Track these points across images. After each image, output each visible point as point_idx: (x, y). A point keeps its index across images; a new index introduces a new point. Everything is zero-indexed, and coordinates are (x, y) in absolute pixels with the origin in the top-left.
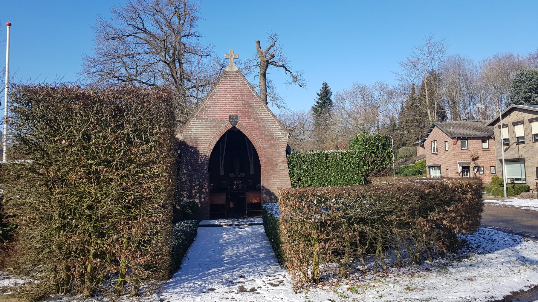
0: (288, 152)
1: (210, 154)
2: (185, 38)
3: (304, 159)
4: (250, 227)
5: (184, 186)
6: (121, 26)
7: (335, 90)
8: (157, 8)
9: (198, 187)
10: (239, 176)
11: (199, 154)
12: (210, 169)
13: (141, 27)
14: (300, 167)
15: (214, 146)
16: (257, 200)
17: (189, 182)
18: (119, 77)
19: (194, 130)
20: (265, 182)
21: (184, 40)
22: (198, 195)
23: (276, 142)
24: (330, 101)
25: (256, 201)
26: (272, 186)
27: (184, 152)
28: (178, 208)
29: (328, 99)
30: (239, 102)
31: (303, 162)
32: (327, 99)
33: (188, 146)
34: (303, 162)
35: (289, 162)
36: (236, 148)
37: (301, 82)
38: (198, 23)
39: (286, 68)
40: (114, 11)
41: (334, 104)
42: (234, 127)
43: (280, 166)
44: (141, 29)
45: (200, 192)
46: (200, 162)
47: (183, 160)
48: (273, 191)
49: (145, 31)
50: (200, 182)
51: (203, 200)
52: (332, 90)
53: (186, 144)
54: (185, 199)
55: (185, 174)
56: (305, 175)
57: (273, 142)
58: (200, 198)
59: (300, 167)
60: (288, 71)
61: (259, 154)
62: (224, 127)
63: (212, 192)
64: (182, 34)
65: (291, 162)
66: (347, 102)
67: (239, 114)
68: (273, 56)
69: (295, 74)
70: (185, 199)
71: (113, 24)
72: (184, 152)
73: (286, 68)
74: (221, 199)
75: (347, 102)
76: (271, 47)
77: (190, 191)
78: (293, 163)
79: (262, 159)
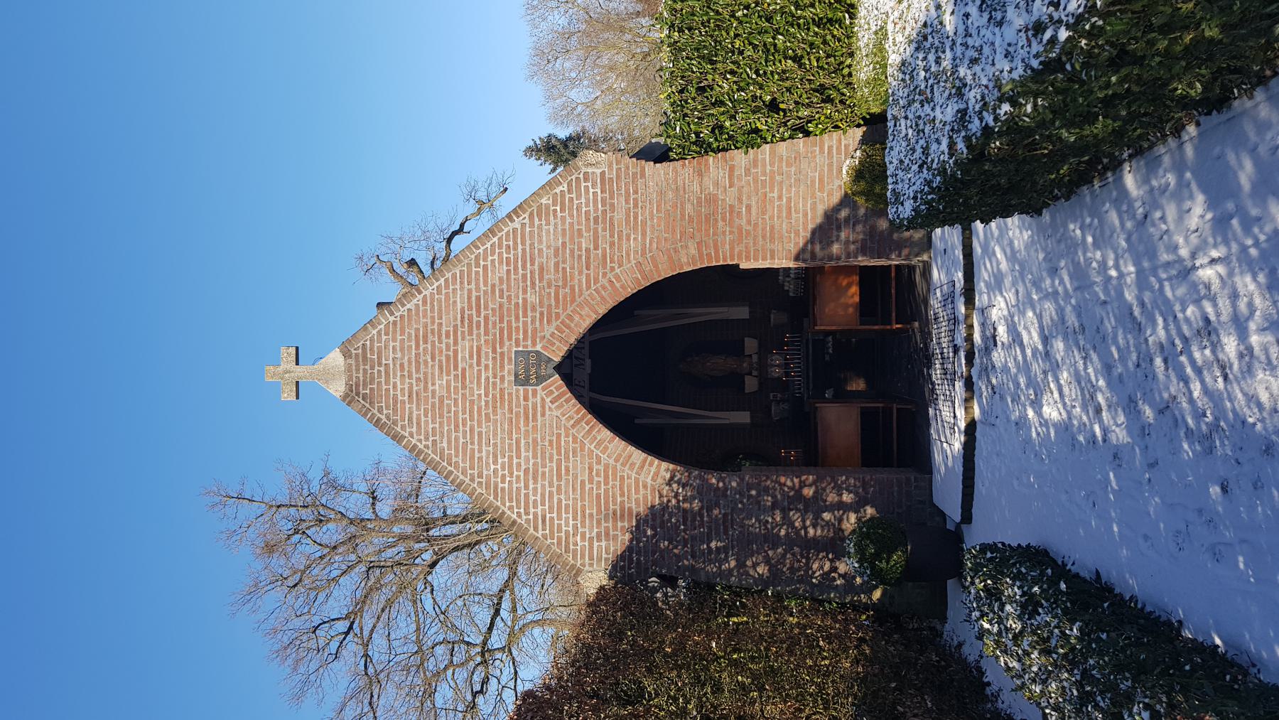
0: (658, 154)
1: (664, 465)
2: (379, 505)
3: (691, 92)
4: (981, 299)
5: (791, 568)
6: (341, 676)
7: (543, 127)
8: (291, 582)
9: (795, 516)
10: (755, 358)
11: (665, 508)
12: (725, 463)
13: (342, 626)
14: (722, 103)
15: (631, 448)
16: (849, 285)
17: (774, 547)
18: (474, 695)
19: (567, 523)
20: (779, 255)
21: (384, 509)
22: (827, 516)
23: (619, 202)
24: (570, 138)
25: (854, 289)
26: (797, 217)
27: (655, 563)
28: (877, 594)
29: (565, 143)
30: (464, 347)
31: (701, 90)
32: (566, 146)
33: (630, 549)
34: (701, 90)
35: (704, 148)
36: (643, 362)
37: (494, 190)
38: (338, 472)
39: (455, 233)
40: (298, 697)
41: (579, 129)
42: (559, 368)
43: (717, 184)
44: (352, 623)
45: (815, 507)
46: (696, 505)
47: (686, 568)
48: (821, 209)
49: (352, 617)
50: (775, 505)
51: (847, 497)
52: (544, 135)
53: (622, 557)
54: (842, 568)
55: (741, 565)
56: (755, 83)
57: (619, 216)
58: (841, 506)
59: (722, 103)
60: (462, 225)
61: (665, 271)
62: (558, 408)
63: (813, 457)
64: (369, 515)
65: (699, 142)
66: (573, 94)
67: (510, 348)
68: (412, 263)
69: (472, 207)
70: (842, 568)
71: (334, 699)
72: (655, 563)
73: (455, 233)
74: (840, 423)
75: (573, 94)
76: (393, 271)
77: (812, 547)
78: (705, 132)
79: (689, 260)
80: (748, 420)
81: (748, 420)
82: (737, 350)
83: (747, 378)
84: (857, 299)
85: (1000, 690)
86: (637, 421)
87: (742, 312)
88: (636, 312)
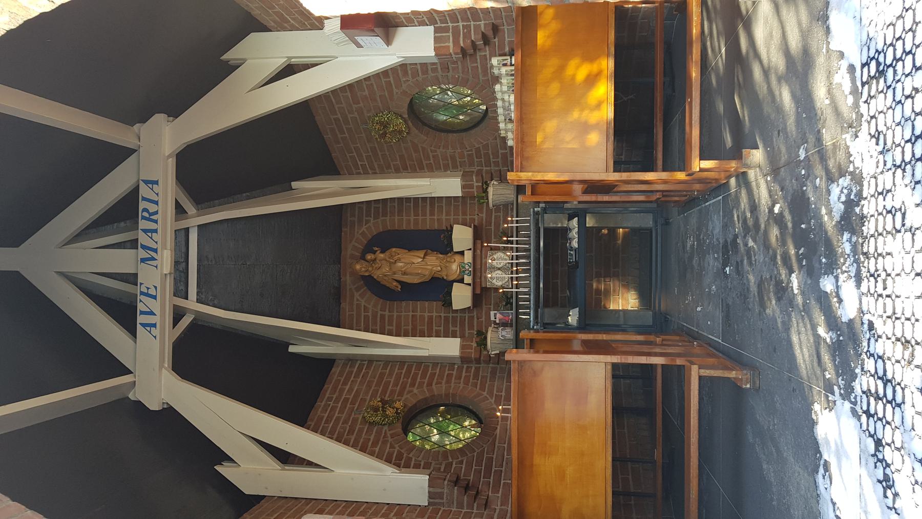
10: (468, 257)
25: (604, 91)
80: (422, 500)
81: (422, 500)
82: (441, 243)
83: (456, 287)
84: (608, 112)
85: (826, 434)
86: (292, 349)
87: (449, 186)
88: (294, 184)
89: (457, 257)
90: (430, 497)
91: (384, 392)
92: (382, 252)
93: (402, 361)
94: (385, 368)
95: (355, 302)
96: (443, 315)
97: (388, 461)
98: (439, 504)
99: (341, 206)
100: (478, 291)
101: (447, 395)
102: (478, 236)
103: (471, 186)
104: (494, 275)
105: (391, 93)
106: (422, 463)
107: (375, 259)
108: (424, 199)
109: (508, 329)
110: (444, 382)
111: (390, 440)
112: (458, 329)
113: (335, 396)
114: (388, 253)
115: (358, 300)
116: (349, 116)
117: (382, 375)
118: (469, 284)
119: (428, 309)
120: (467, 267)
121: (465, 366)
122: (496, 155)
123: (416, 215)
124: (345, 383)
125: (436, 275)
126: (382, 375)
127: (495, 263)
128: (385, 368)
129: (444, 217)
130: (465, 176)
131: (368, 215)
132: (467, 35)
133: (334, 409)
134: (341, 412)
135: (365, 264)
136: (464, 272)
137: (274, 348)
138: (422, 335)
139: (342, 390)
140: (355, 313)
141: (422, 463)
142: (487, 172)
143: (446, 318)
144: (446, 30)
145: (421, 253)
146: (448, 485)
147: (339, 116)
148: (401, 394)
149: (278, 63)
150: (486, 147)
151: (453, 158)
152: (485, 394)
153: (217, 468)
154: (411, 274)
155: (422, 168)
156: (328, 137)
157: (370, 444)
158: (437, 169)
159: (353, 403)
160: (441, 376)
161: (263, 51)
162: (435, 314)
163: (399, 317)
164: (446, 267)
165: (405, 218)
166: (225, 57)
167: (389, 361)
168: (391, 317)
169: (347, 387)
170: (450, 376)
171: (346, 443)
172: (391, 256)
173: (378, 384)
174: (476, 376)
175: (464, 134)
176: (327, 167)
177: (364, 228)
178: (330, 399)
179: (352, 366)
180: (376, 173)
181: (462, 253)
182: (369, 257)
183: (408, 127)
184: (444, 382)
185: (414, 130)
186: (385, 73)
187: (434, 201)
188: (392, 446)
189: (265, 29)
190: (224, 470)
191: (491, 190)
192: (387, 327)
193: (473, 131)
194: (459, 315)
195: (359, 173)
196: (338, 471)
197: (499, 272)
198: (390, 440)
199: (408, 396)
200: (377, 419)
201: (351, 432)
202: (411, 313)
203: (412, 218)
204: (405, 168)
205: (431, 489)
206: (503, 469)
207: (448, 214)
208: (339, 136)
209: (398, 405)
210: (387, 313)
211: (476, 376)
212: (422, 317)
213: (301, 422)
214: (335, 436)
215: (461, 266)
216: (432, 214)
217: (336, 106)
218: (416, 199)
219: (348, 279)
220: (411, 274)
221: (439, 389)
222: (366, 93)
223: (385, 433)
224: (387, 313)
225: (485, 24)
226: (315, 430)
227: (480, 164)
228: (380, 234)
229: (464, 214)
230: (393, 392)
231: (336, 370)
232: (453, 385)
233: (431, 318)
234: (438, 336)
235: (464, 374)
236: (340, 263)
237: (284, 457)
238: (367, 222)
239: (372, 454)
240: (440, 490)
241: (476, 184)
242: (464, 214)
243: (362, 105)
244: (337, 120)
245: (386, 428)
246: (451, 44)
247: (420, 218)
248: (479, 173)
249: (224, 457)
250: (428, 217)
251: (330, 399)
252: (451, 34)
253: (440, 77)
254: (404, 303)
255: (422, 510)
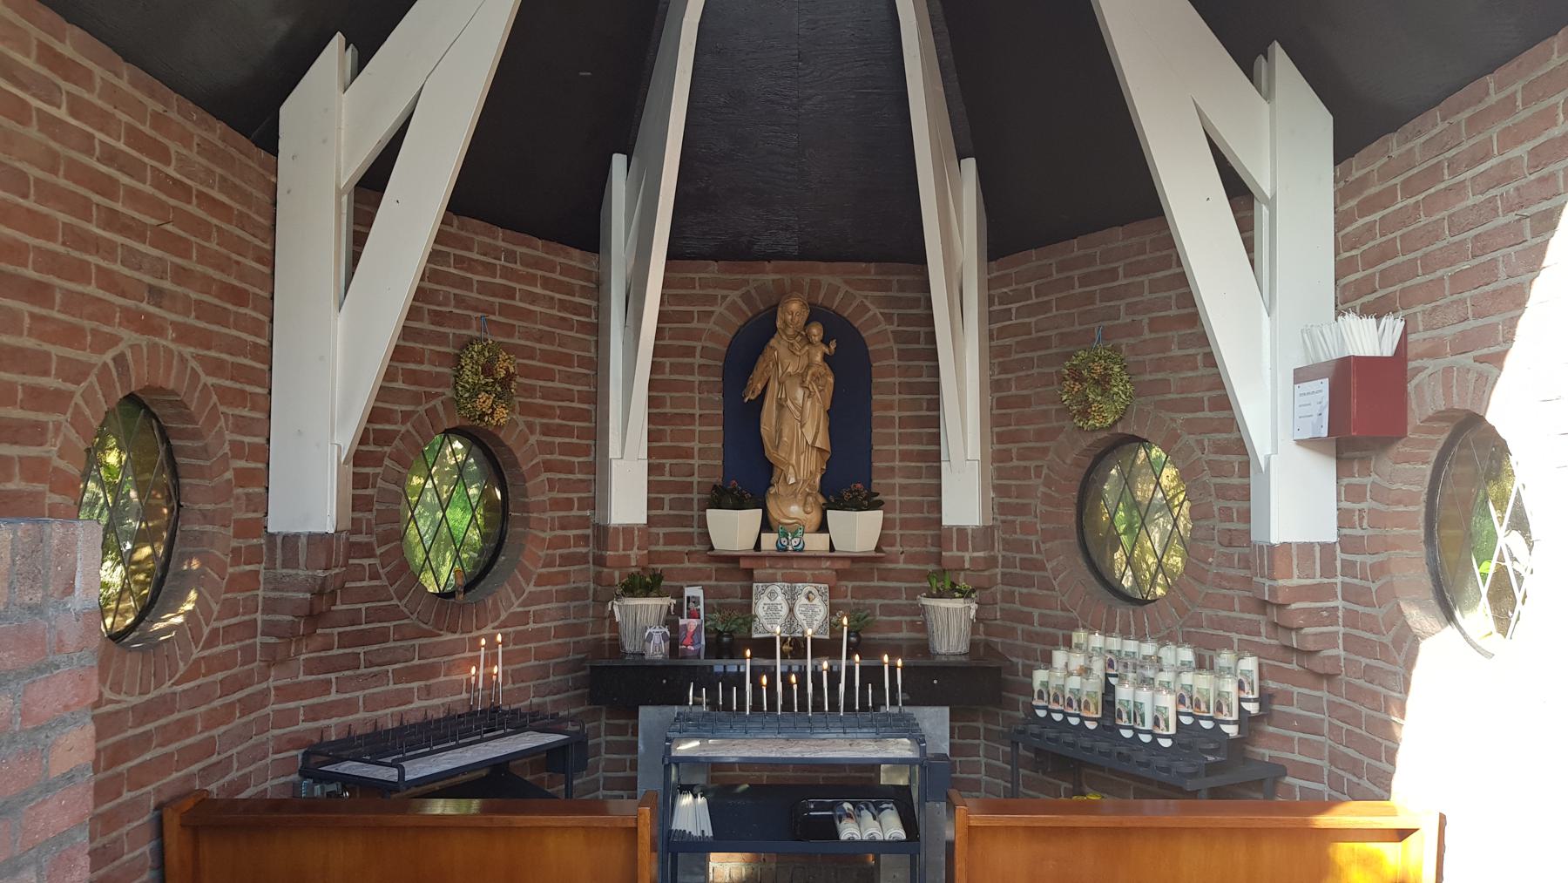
10: (816, 543)
82: (845, 485)
86: (619, 160)
87: (964, 501)
88: (970, 165)
89: (815, 517)
90: (286, 537)
91: (527, 372)
92: (826, 358)
93: (596, 397)
94: (583, 362)
95: (720, 292)
96: (695, 479)
97: (375, 415)
98: (272, 560)
99: (922, 260)
100: (743, 564)
101: (525, 508)
102: (857, 566)
103: (962, 546)
104: (780, 599)
105: (1175, 406)
106: (369, 492)
107: (810, 343)
108: (936, 440)
109: (665, 647)
110: (555, 494)
111: (421, 409)
112: (666, 511)
113: (518, 266)
114: (824, 369)
115: (724, 297)
116: (1122, 304)
117: (566, 360)
118: (758, 546)
119: (706, 452)
120: (795, 542)
121: (589, 532)
122: (1028, 600)
123: (903, 422)
124: (546, 283)
125: (776, 473)
126: (566, 360)
127: (802, 600)
128: (583, 362)
129: (898, 481)
130: (986, 533)
131: (903, 320)
132: (1314, 617)
133: (490, 269)
134: (484, 288)
135: (801, 319)
136: (786, 536)
137: (621, 123)
138: (652, 436)
139: (531, 280)
140: (697, 291)
141: (369, 492)
142: (992, 578)
143: (688, 487)
144: (1328, 570)
145: (823, 442)
146: (314, 578)
147: (1122, 281)
148: (526, 409)
149: (1259, 172)
150: (1046, 584)
151: (1023, 509)
152: (531, 588)
153: (338, 39)
154: (779, 418)
155: (1001, 438)
156: (1075, 248)
157: (412, 366)
158: (998, 470)
159: (504, 311)
160: (567, 486)
161: (1290, 138)
162: (696, 462)
163: (688, 386)
164: (795, 494)
165: (897, 397)
166: (1278, 51)
167: (597, 367)
168: (689, 369)
169: (538, 290)
170: (568, 504)
171: (413, 313)
172: (816, 378)
173: (547, 356)
174: (567, 560)
175: (1074, 540)
176: (1004, 238)
177: (874, 310)
178: (511, 256)
179: (584, 292)
180: (991, 338)
181: (823, 527)
182: (816, 331)
183: (1094, 430)
184: (555, 494)
185: (1090, 440)
186: (1223, 402)
187: (931, 460)
188: (406, 416)
189: (1343, 152)
190: (335, 54)
191: (957, 604)
192: (667, 361)
193: (1081, 561)
194: (695, 530)
195: (991, 303)
196: (340, 323)
197: (784, 611)
198: (421, 409)
199: (522, 426)
200: (468, 376)
201: (438, 318)
202: (697, 412)
203: (896, 414)
204: (1001, 403)
205: (304, 540)
206: (363, 670)
207: (904, 489)
208: (1076, 273)
209: (502, 415)
210: (698, 360)
211: (567, 560)
212: (690, 436)
213: (462, 203)
214: (427, 285)
215: (796, 529)
216: (905, 456)
217: (1145, 279)
218: (936, 422)
219: (768, 275)
220: (779, 418)
221: (539, 490)
222: (1175, 352)
223: (438, 395)
224: (698, 360)
225: (1337, 658)
226: (440, 238)
227: (1008, 563)
228: (862, 344)
229: (905, 524)
230: (529, 390)
231: (575, 258)
232: (547, 515)
233: (688, 454)
234: (652, 469)
235: (571, 533)
236: (801, 258)
237: (372, 184)
238: (888, 318)
239: (389, 375)
240: (302, 559)
241: (967, 556)
242: (905, 524)
243: (1147, 335)
244: (1113, 274)
245: (449, 393)
246: (1295, 581)
247: (897, 431)
248: (991, 562)
249: (366, 47)
250: (898, 447)
251: (511, 256)
252: (1318, 580)
253: (1210, 523)
254: (718, 397)
255: (258, 526)
